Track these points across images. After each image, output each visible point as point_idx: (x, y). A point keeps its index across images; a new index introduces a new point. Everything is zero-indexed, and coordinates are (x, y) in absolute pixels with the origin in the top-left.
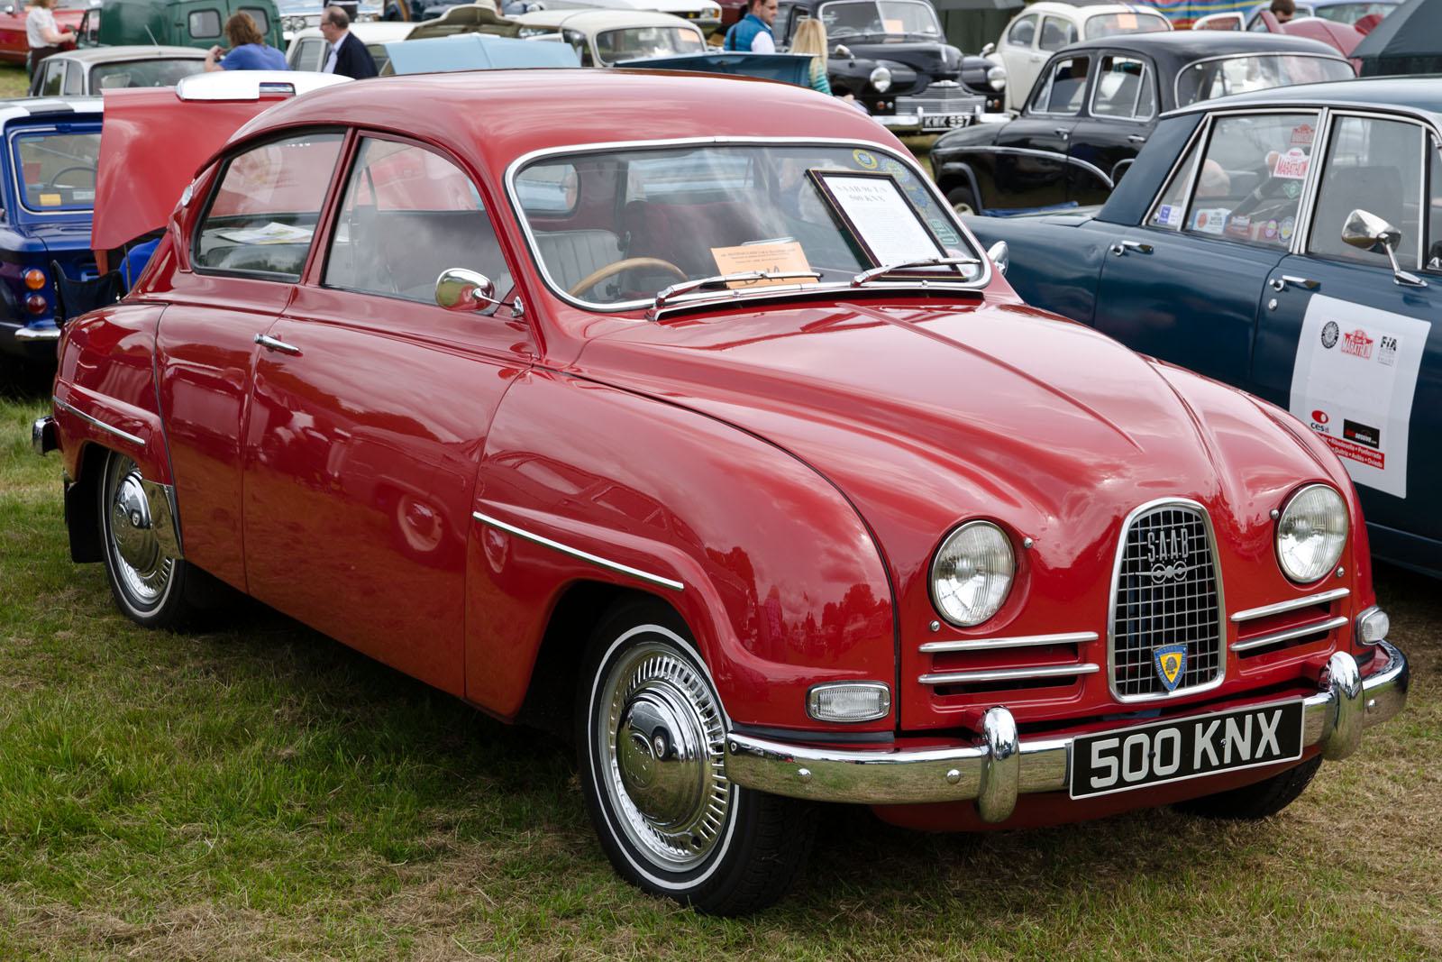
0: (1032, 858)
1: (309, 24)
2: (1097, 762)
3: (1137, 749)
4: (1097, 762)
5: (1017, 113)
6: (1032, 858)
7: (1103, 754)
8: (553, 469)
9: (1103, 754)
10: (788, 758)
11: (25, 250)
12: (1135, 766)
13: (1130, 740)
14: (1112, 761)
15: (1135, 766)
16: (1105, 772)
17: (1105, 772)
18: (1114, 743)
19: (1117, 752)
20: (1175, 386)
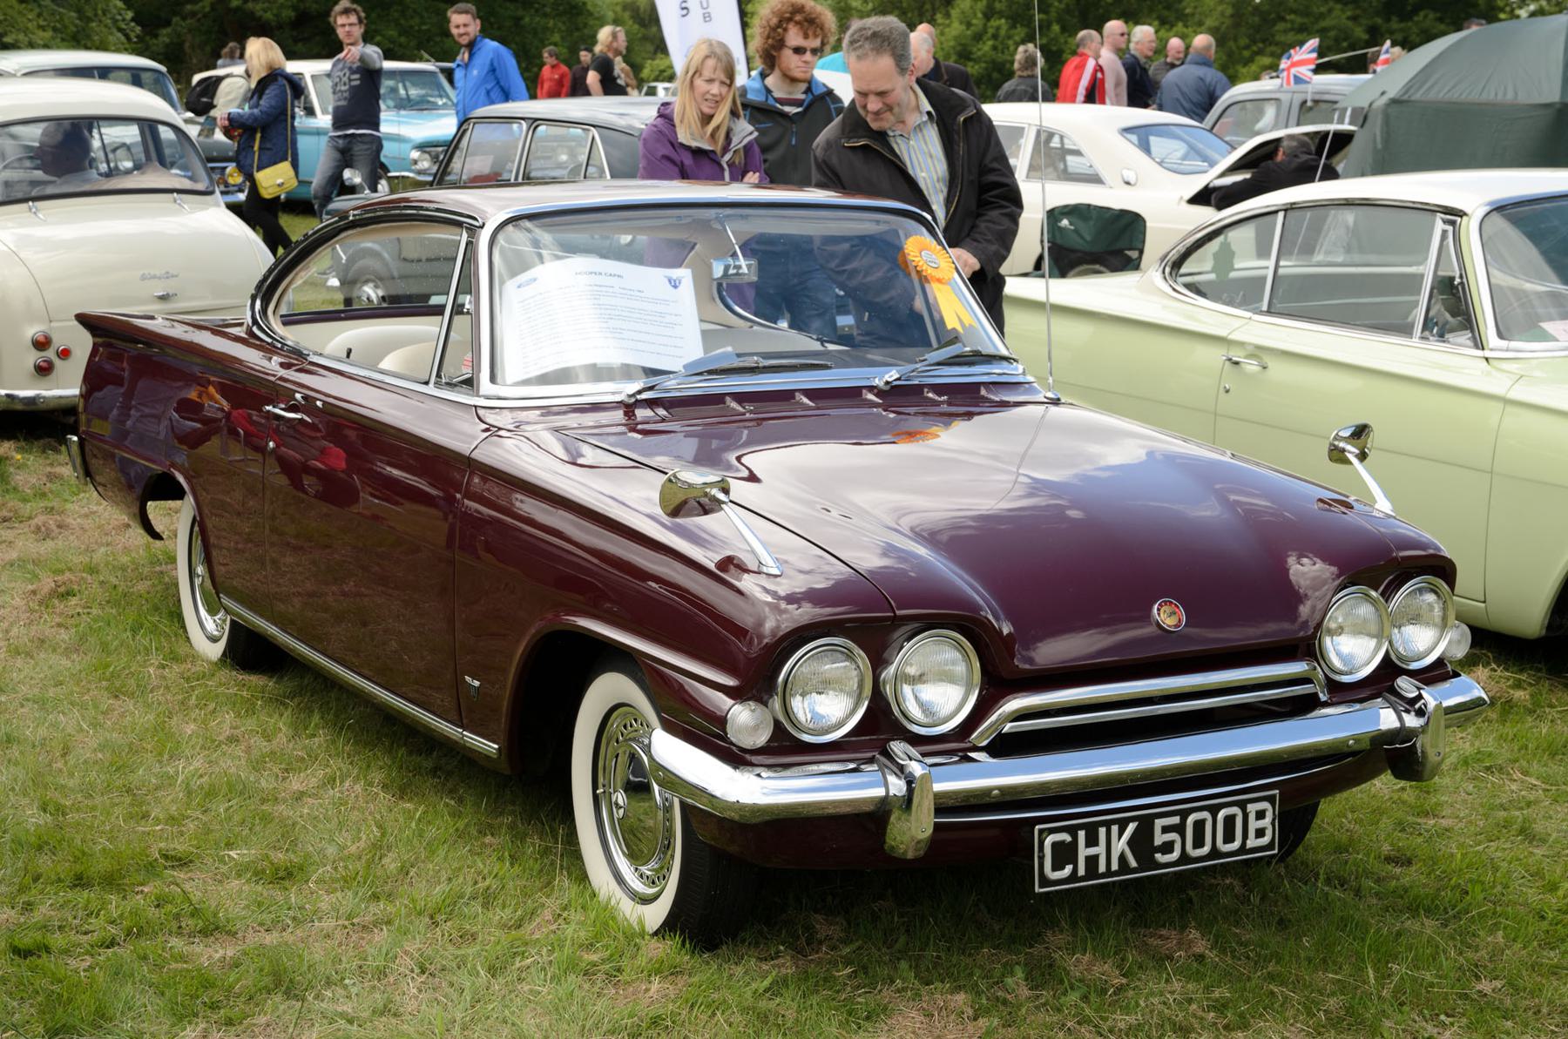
0: (402, 92)
1: (619, 415)
2: (1160, 839)
3: (1199, 825)
4: (1160, 839)
5: (1406, 686)
6: (402, 92)
7: (1165, 830)
8: (769, 767)
9: (1165, 830)
10: (668, 846)
11: (916, 423)
12: (1198, 843)
13: (1236, 845)
14: (1173, 836)
15: (1198, 843)
16: (1167, 847)
17: (1167, 847)
18: (1176, 820)
19: (1180, 829)
20: (664, 436)
